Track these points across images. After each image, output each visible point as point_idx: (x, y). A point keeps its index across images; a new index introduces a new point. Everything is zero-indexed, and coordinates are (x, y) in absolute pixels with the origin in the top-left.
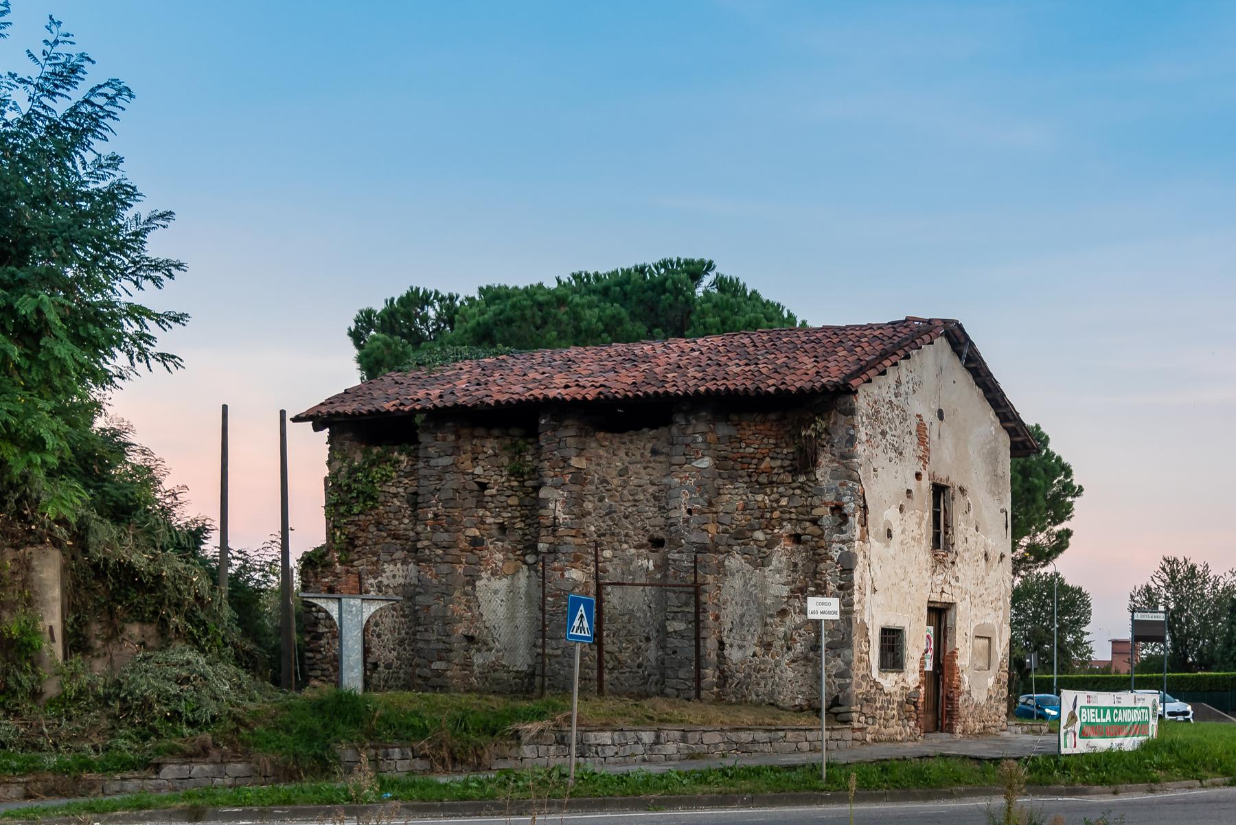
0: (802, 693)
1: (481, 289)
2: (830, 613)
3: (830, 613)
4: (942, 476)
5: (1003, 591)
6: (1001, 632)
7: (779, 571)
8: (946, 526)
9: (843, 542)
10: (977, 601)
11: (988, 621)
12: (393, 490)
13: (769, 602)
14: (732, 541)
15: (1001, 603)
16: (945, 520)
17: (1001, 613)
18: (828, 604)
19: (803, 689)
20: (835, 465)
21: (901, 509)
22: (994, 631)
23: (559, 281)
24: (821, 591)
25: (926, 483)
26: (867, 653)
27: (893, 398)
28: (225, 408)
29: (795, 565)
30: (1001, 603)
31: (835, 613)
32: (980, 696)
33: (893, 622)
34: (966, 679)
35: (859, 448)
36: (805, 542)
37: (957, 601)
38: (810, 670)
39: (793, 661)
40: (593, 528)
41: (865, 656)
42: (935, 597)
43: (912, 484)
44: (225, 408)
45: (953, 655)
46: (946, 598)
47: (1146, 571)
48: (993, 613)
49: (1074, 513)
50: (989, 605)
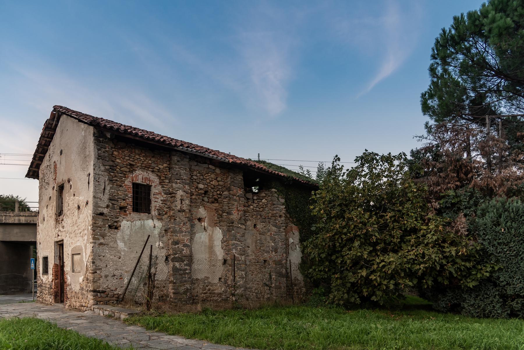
5: (87, 224)
6: (86, 249)
10: (72, 236)
11: (78, 244)
15: (86, 232)
17: (86, 238)
22: (82, 249)
23: (17, 197)
24: (324, 258)
28: (149, 236)
30: (86, 232)
32: (76, 288)
34: (69, 278)
37: (64, 238)
42: (57, 239)
44: (149, 236)
46: (60, 238)
47: (452, 22)
48: (81, 239)
49: (15, 196)
50: (79, 235)
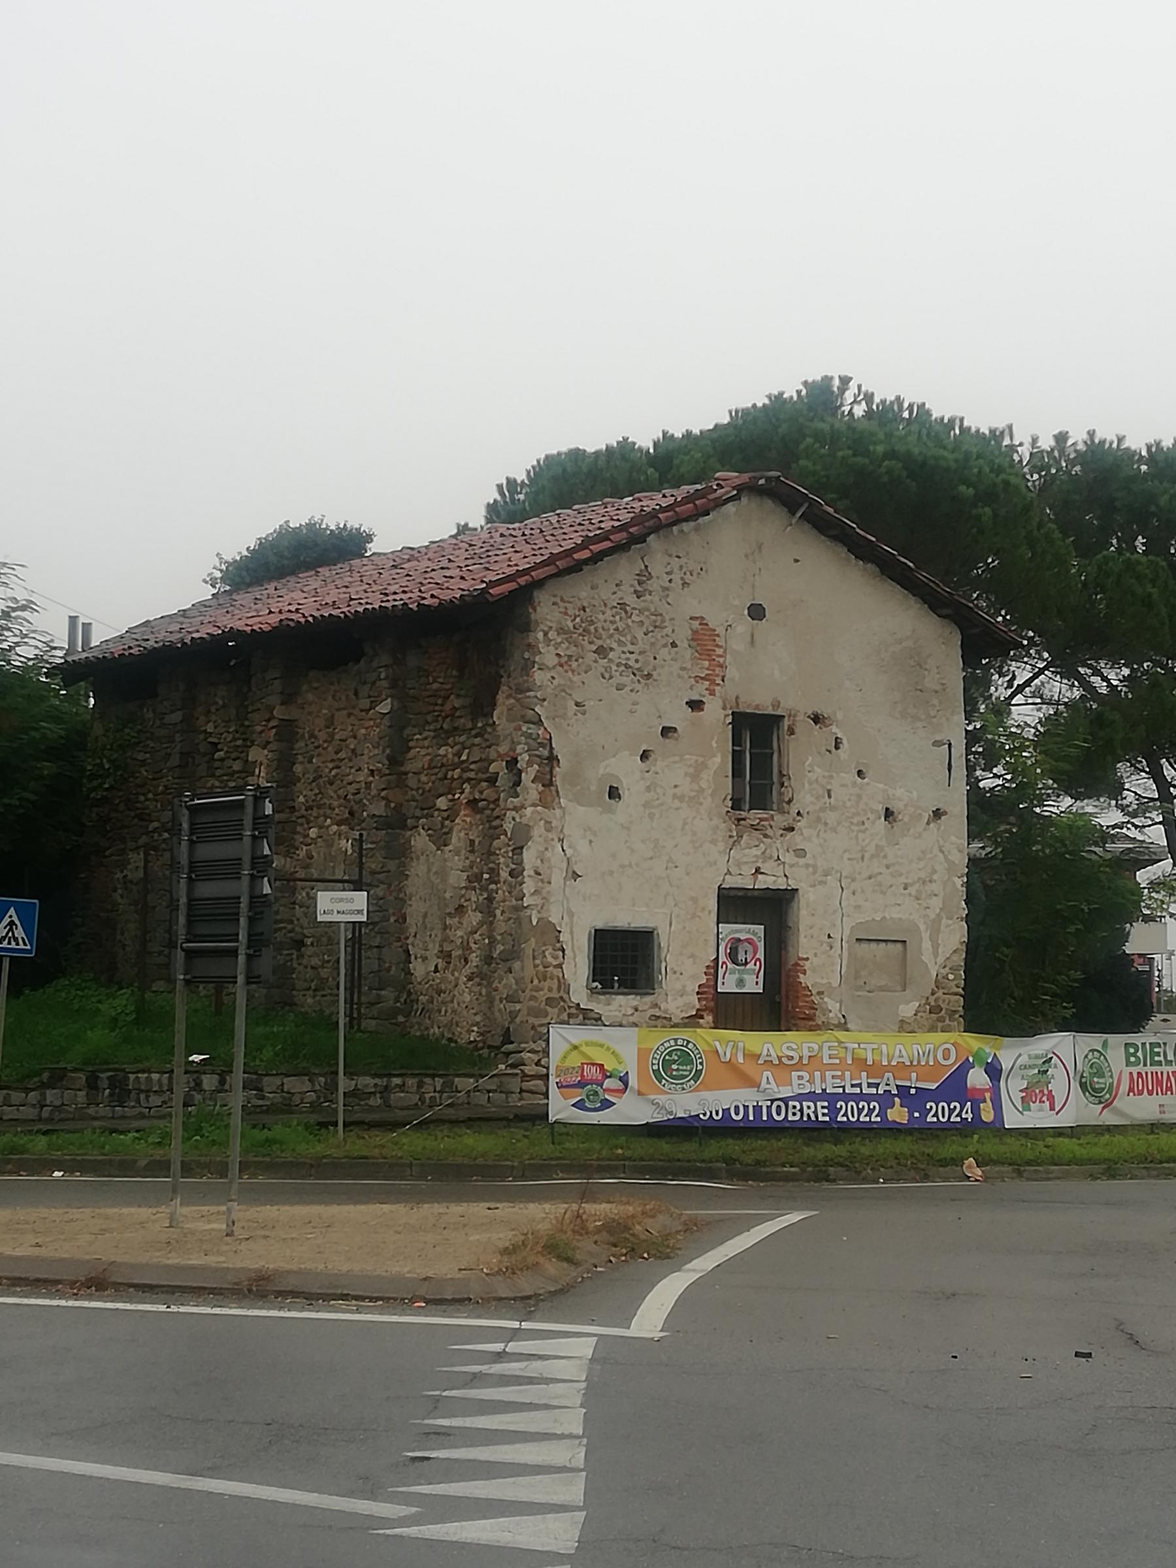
0: (477, 1024)
1: (507, 478)
2: (351, 912)
3: (351, 912)
4: (759, 700)
7: (458, 853)
8: (781, 775)
9: (515, 809)
12: (141, 756)
13: (448, 895)
14: (418, 813)
16: (780, 766)
18: (352, 900)
19: (478, 1018)
20: (512, 701)
21: (645, 756)
25: (716, 715)
26: (560, 966)
27: (631, 600)
29: (472, 842)
31: (360, 912)
33: (625, 917)
35: (539, 677)
36: (481, 811)
38: (484, 992)
39: (470, 979)
40: (301, 799)
41: (557, 972)
43: (679, 717)
45: (798, 968)
